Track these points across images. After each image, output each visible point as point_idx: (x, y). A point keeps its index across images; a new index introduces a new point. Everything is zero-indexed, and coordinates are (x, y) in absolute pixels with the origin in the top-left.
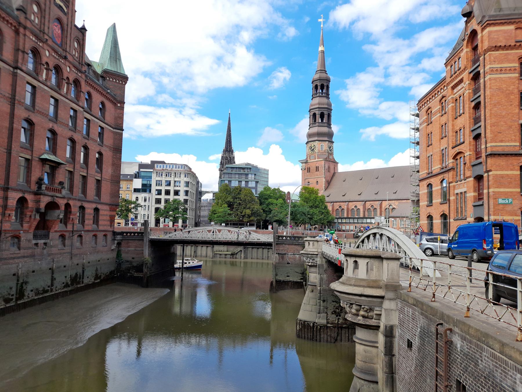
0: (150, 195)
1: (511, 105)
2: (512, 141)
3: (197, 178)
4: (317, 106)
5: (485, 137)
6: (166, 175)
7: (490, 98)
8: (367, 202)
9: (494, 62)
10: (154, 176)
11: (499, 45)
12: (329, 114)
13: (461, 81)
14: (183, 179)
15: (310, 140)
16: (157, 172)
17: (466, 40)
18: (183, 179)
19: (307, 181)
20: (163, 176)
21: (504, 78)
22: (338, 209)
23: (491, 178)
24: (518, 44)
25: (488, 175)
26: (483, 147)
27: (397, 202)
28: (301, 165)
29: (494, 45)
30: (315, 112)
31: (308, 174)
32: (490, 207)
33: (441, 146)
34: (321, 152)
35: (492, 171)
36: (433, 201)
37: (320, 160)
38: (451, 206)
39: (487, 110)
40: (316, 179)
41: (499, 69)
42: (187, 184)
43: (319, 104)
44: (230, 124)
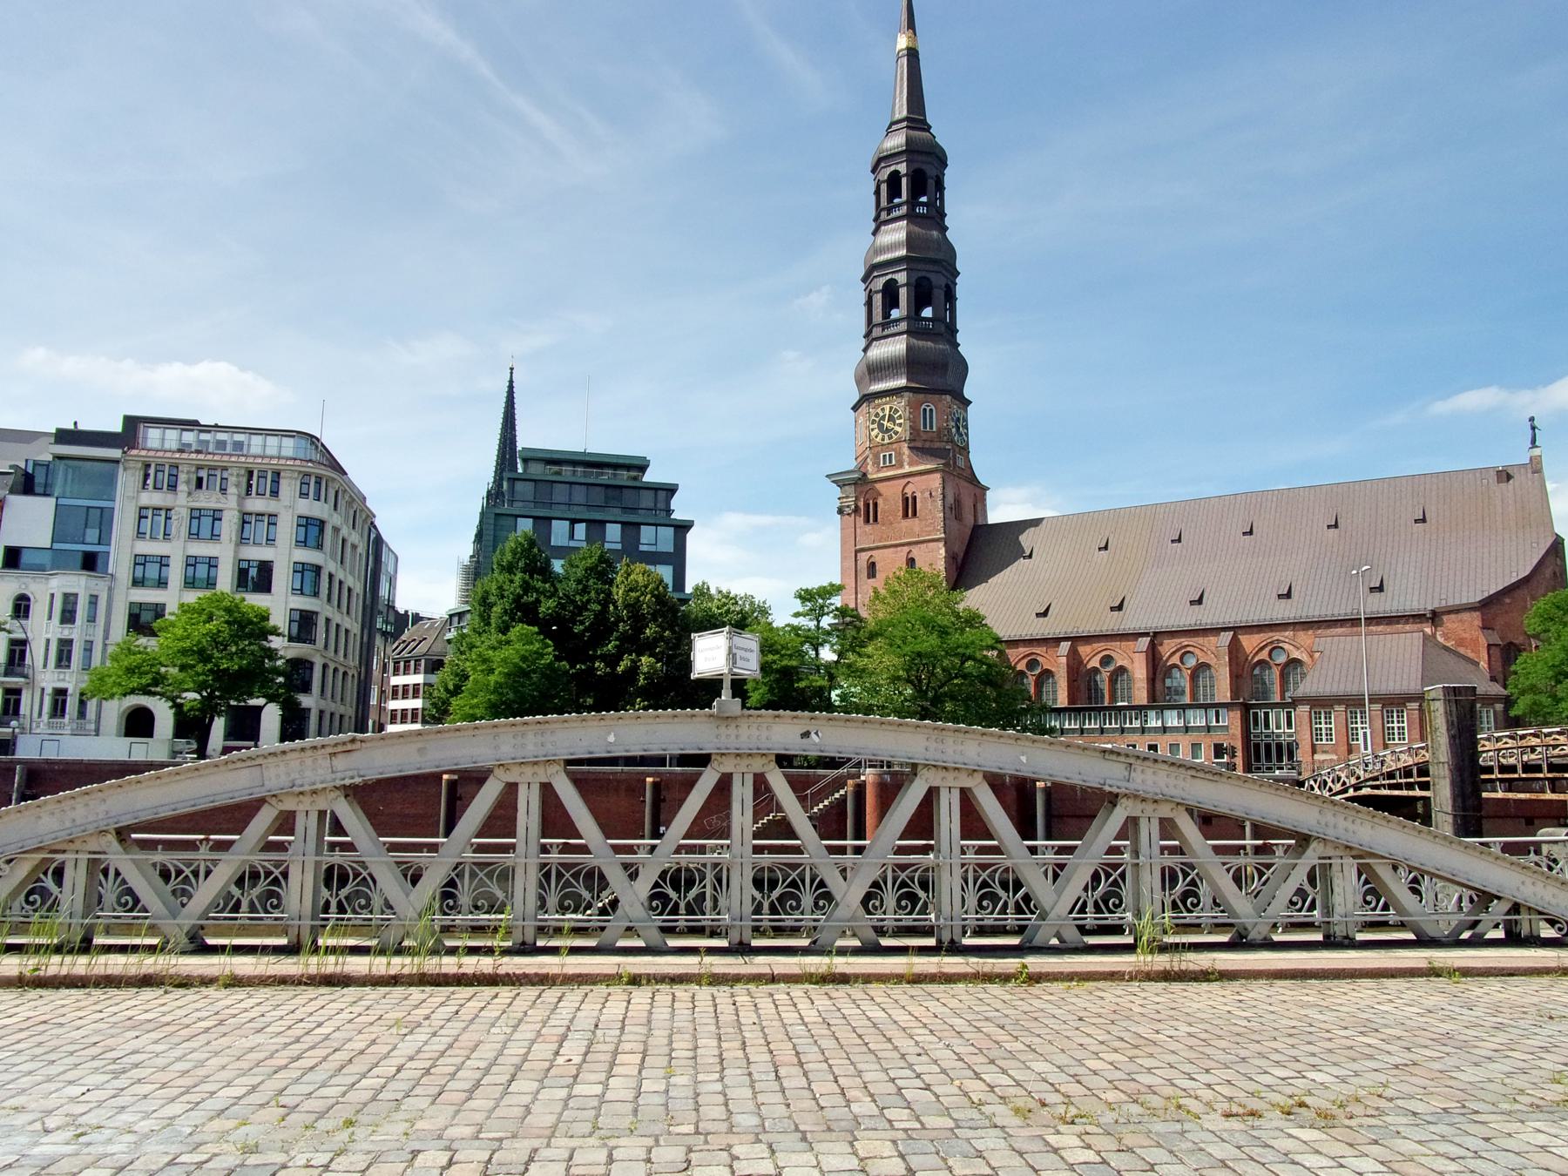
0: (99, 586)
3: (370, 517)
6: (200, 481)
10: (127, 481)
12: (947, 286)
14: (291, 506)
16: (148, 466)
18: (291, 506)
19: (864, 557)
20: (182, 487)
27: (1305, 637)
28: (837, 492)
30: (894, 276)
31: (868, 528)
34: (924, 437)
40: (906, 549)
42: (312, 531)
44: (513, 403)
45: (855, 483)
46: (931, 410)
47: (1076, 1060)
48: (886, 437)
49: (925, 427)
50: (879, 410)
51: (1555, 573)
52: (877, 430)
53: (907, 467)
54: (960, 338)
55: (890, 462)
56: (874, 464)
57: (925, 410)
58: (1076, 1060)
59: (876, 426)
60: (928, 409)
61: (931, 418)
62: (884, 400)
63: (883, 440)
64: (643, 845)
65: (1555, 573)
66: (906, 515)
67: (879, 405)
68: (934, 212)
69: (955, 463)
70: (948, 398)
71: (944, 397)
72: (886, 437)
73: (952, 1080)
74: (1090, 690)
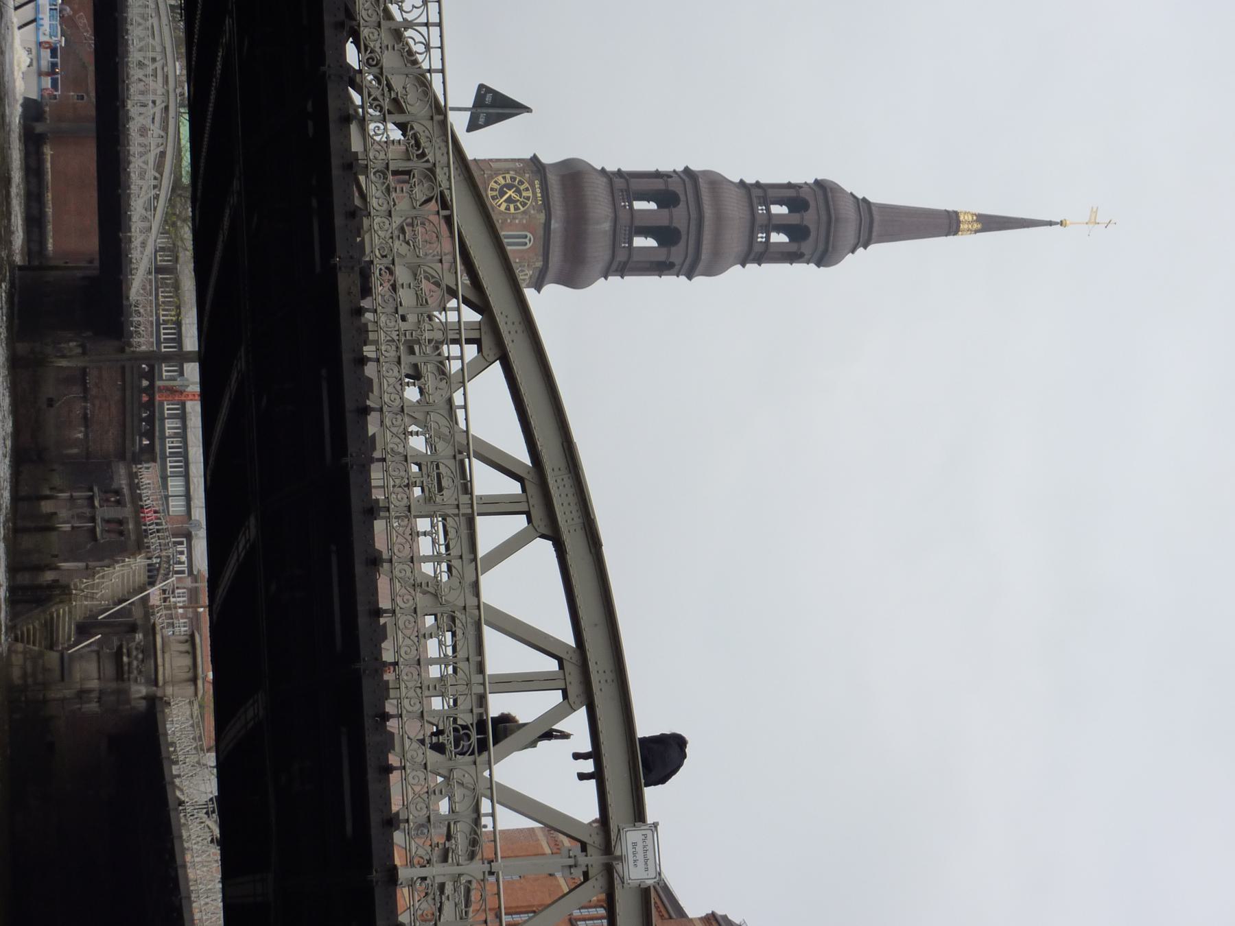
11: (415, 437)
15: (553, 180)
50: (526, 185)
52: (503, 182)
54: (614, 280)
57: (526, 237)
59: (509, 181)
60: (527, 240)
62: (538, 191)
63: (492, 189)
67: (533, 186)
70: (539, 264)
71: (541, 258)
72: (494, 193)
73: (419, 796)
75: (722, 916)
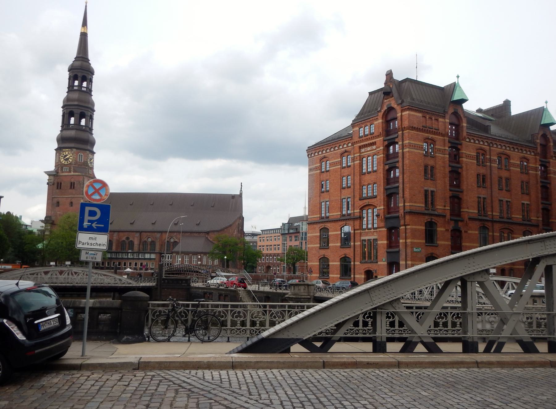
1: (420, 174)
2: (419, 203)
4: (76, 103)
5: (403, 197)
7: (409, 167)
8: (142, 234)
9: (411, 139)
11: (414, 126)
13: (374, 144)
17: (382, 113)
21: (417, 152)
22: (124, 241)
23: (408, 231)
24: (424, 129)
25: (406, 229)
26: (401, 205)
29: (412, 126)
31: (58, 191)
32: (407, 254)
33: (342, 195)
34: (79, 164)
35: (410, 225)
36: (330, 245)
37: (77, 174)
38: (356, 251)
39: (405, 176)
41: (414, 145)
43: (78, 100)
45: (54, 175)
46: (82, 155)
47: (362, 404)
48: (66, 162)
49: (79, 160)
51: (239, 224)
52: (63, 159)
53: (72, 173)
55: (67, 170)
56: (61, 170)
57: (80, 155)
58: (362, 404)
61: (82, 157)
62: (66, 150)
63: (65, 163)
64: (249, 304)
65: (239, 224)
66: (71, 188)
68: (88, 91)
69: (88, 172)
72: (66, 162)
74: (122, 246)
75: (353, 122)
